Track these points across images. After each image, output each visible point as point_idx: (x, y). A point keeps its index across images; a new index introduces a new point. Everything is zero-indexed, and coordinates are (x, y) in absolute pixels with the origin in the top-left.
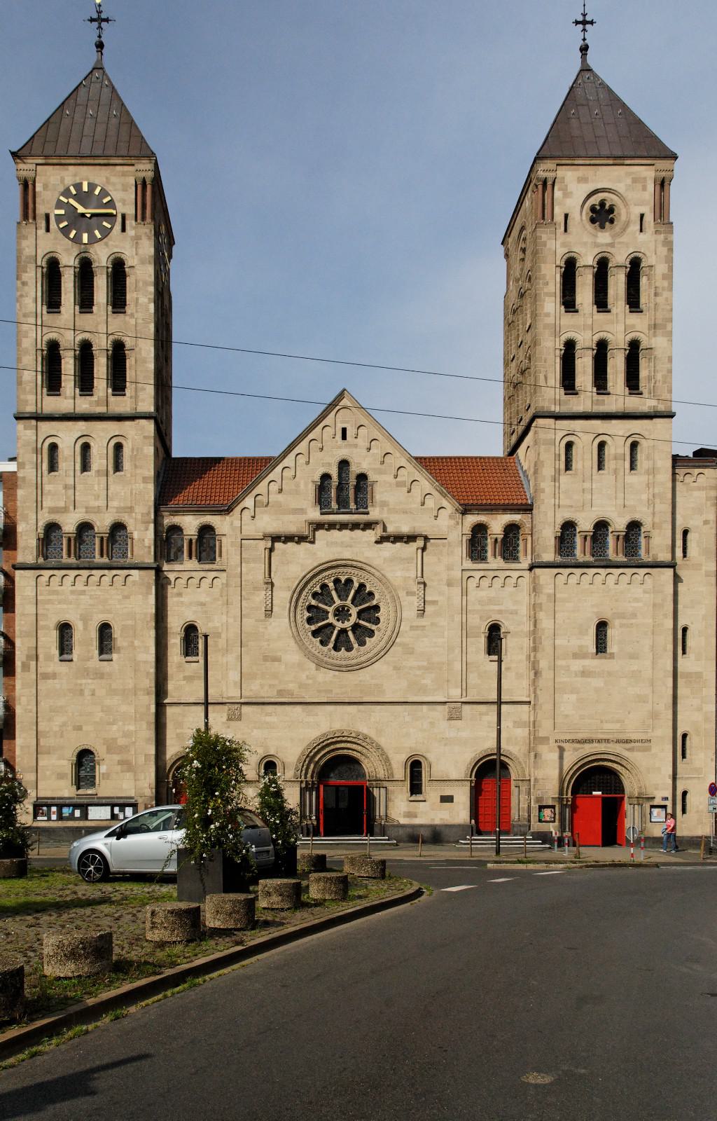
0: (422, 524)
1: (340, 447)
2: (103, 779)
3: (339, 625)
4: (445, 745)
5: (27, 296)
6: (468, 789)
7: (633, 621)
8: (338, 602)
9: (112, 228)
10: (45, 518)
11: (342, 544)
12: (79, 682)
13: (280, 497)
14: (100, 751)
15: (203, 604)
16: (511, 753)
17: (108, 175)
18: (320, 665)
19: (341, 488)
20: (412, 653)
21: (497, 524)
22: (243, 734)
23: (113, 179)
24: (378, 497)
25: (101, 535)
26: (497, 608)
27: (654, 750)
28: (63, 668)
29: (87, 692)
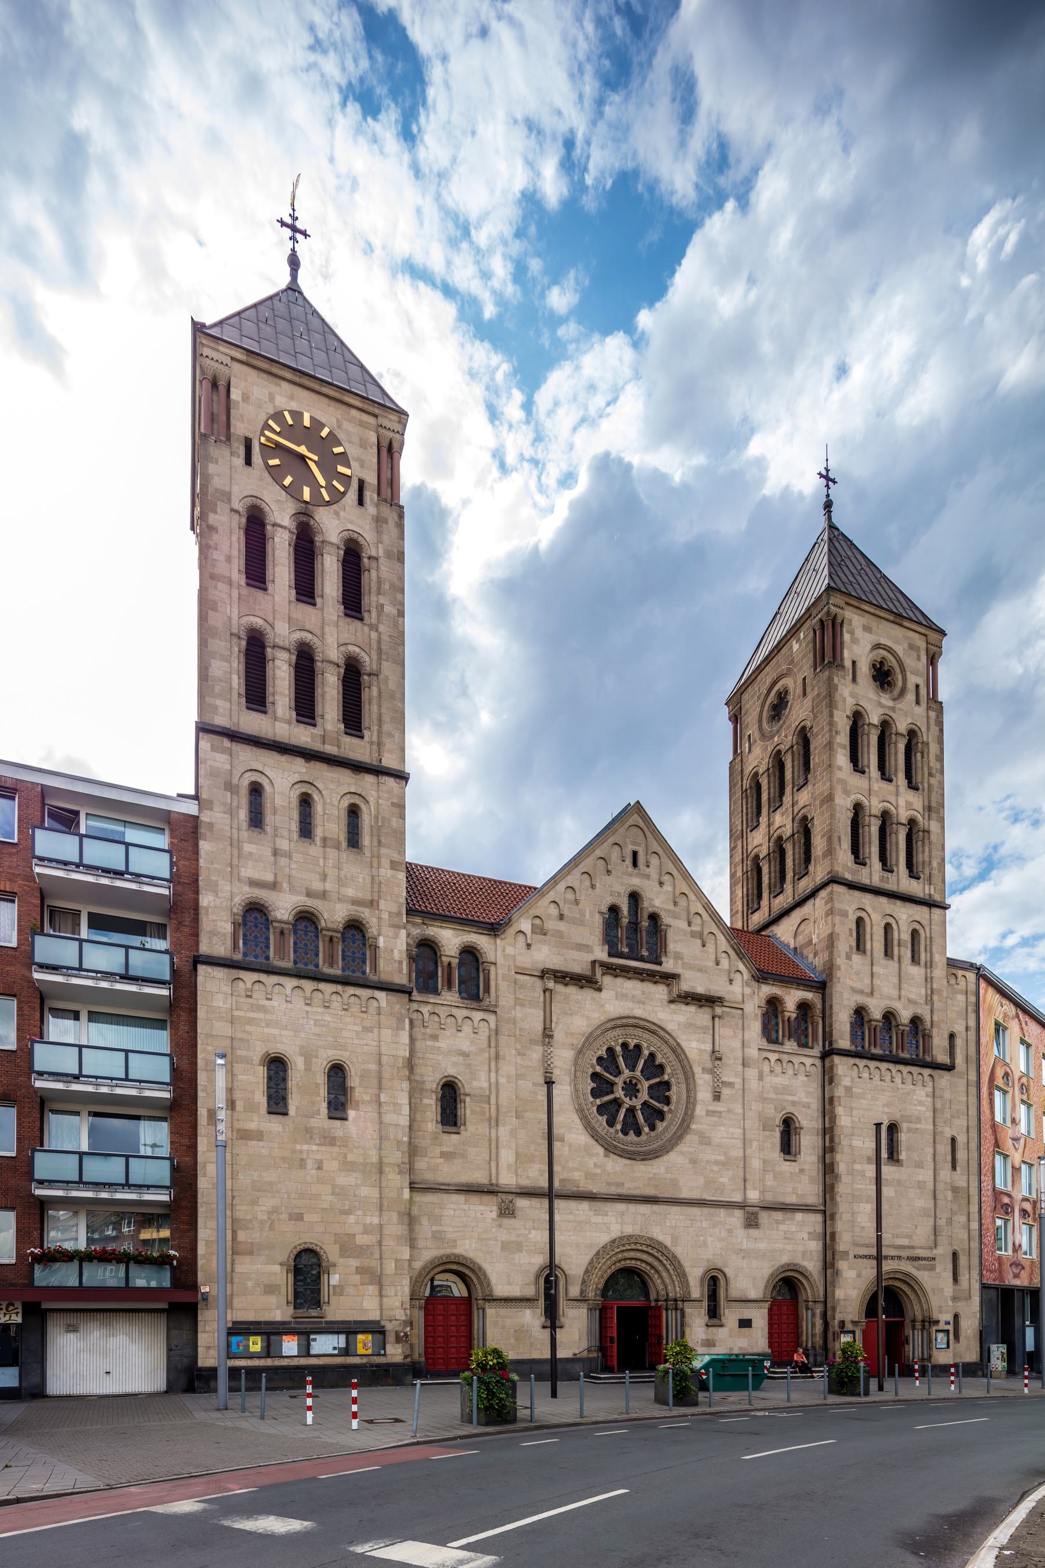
0: (717, 986)
1: (631, 875)
2: (334, 1294)
3: (628, 1102)
4: (744, 1258)
5: (216, 549)
6: (766, 1311)
7: (918, 1126)
8: (627, 1073)
9: (344, 494)
10: (245, 893)
11: (634, 999)
12: (298, 1147)
13: (562, 926)
14: (331, 1252)
15: (465, 1055)
16: (806, 1270)
17: (340, 417)
18: (610, 1149)
19: (634, 925)
20: (709, 1144)
21: (792, 998)
22: (518, 1236)
23: (346, 425)
24: (672, 946)
25: (330, 933)
26: (791, 1098)
27: (938, 1270)
28: (274, 1125)
29: (310, 1164)
